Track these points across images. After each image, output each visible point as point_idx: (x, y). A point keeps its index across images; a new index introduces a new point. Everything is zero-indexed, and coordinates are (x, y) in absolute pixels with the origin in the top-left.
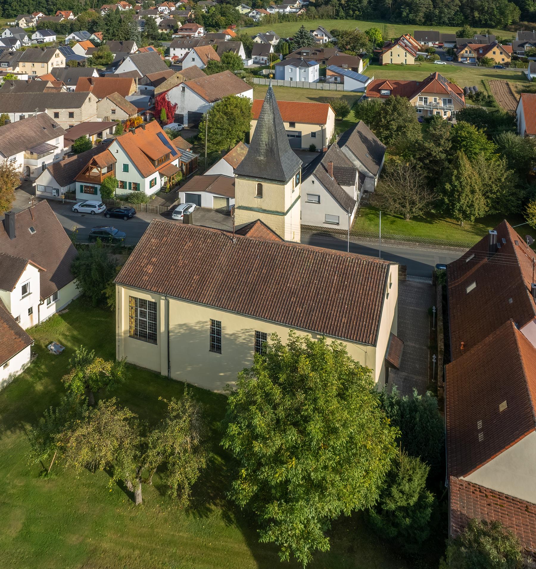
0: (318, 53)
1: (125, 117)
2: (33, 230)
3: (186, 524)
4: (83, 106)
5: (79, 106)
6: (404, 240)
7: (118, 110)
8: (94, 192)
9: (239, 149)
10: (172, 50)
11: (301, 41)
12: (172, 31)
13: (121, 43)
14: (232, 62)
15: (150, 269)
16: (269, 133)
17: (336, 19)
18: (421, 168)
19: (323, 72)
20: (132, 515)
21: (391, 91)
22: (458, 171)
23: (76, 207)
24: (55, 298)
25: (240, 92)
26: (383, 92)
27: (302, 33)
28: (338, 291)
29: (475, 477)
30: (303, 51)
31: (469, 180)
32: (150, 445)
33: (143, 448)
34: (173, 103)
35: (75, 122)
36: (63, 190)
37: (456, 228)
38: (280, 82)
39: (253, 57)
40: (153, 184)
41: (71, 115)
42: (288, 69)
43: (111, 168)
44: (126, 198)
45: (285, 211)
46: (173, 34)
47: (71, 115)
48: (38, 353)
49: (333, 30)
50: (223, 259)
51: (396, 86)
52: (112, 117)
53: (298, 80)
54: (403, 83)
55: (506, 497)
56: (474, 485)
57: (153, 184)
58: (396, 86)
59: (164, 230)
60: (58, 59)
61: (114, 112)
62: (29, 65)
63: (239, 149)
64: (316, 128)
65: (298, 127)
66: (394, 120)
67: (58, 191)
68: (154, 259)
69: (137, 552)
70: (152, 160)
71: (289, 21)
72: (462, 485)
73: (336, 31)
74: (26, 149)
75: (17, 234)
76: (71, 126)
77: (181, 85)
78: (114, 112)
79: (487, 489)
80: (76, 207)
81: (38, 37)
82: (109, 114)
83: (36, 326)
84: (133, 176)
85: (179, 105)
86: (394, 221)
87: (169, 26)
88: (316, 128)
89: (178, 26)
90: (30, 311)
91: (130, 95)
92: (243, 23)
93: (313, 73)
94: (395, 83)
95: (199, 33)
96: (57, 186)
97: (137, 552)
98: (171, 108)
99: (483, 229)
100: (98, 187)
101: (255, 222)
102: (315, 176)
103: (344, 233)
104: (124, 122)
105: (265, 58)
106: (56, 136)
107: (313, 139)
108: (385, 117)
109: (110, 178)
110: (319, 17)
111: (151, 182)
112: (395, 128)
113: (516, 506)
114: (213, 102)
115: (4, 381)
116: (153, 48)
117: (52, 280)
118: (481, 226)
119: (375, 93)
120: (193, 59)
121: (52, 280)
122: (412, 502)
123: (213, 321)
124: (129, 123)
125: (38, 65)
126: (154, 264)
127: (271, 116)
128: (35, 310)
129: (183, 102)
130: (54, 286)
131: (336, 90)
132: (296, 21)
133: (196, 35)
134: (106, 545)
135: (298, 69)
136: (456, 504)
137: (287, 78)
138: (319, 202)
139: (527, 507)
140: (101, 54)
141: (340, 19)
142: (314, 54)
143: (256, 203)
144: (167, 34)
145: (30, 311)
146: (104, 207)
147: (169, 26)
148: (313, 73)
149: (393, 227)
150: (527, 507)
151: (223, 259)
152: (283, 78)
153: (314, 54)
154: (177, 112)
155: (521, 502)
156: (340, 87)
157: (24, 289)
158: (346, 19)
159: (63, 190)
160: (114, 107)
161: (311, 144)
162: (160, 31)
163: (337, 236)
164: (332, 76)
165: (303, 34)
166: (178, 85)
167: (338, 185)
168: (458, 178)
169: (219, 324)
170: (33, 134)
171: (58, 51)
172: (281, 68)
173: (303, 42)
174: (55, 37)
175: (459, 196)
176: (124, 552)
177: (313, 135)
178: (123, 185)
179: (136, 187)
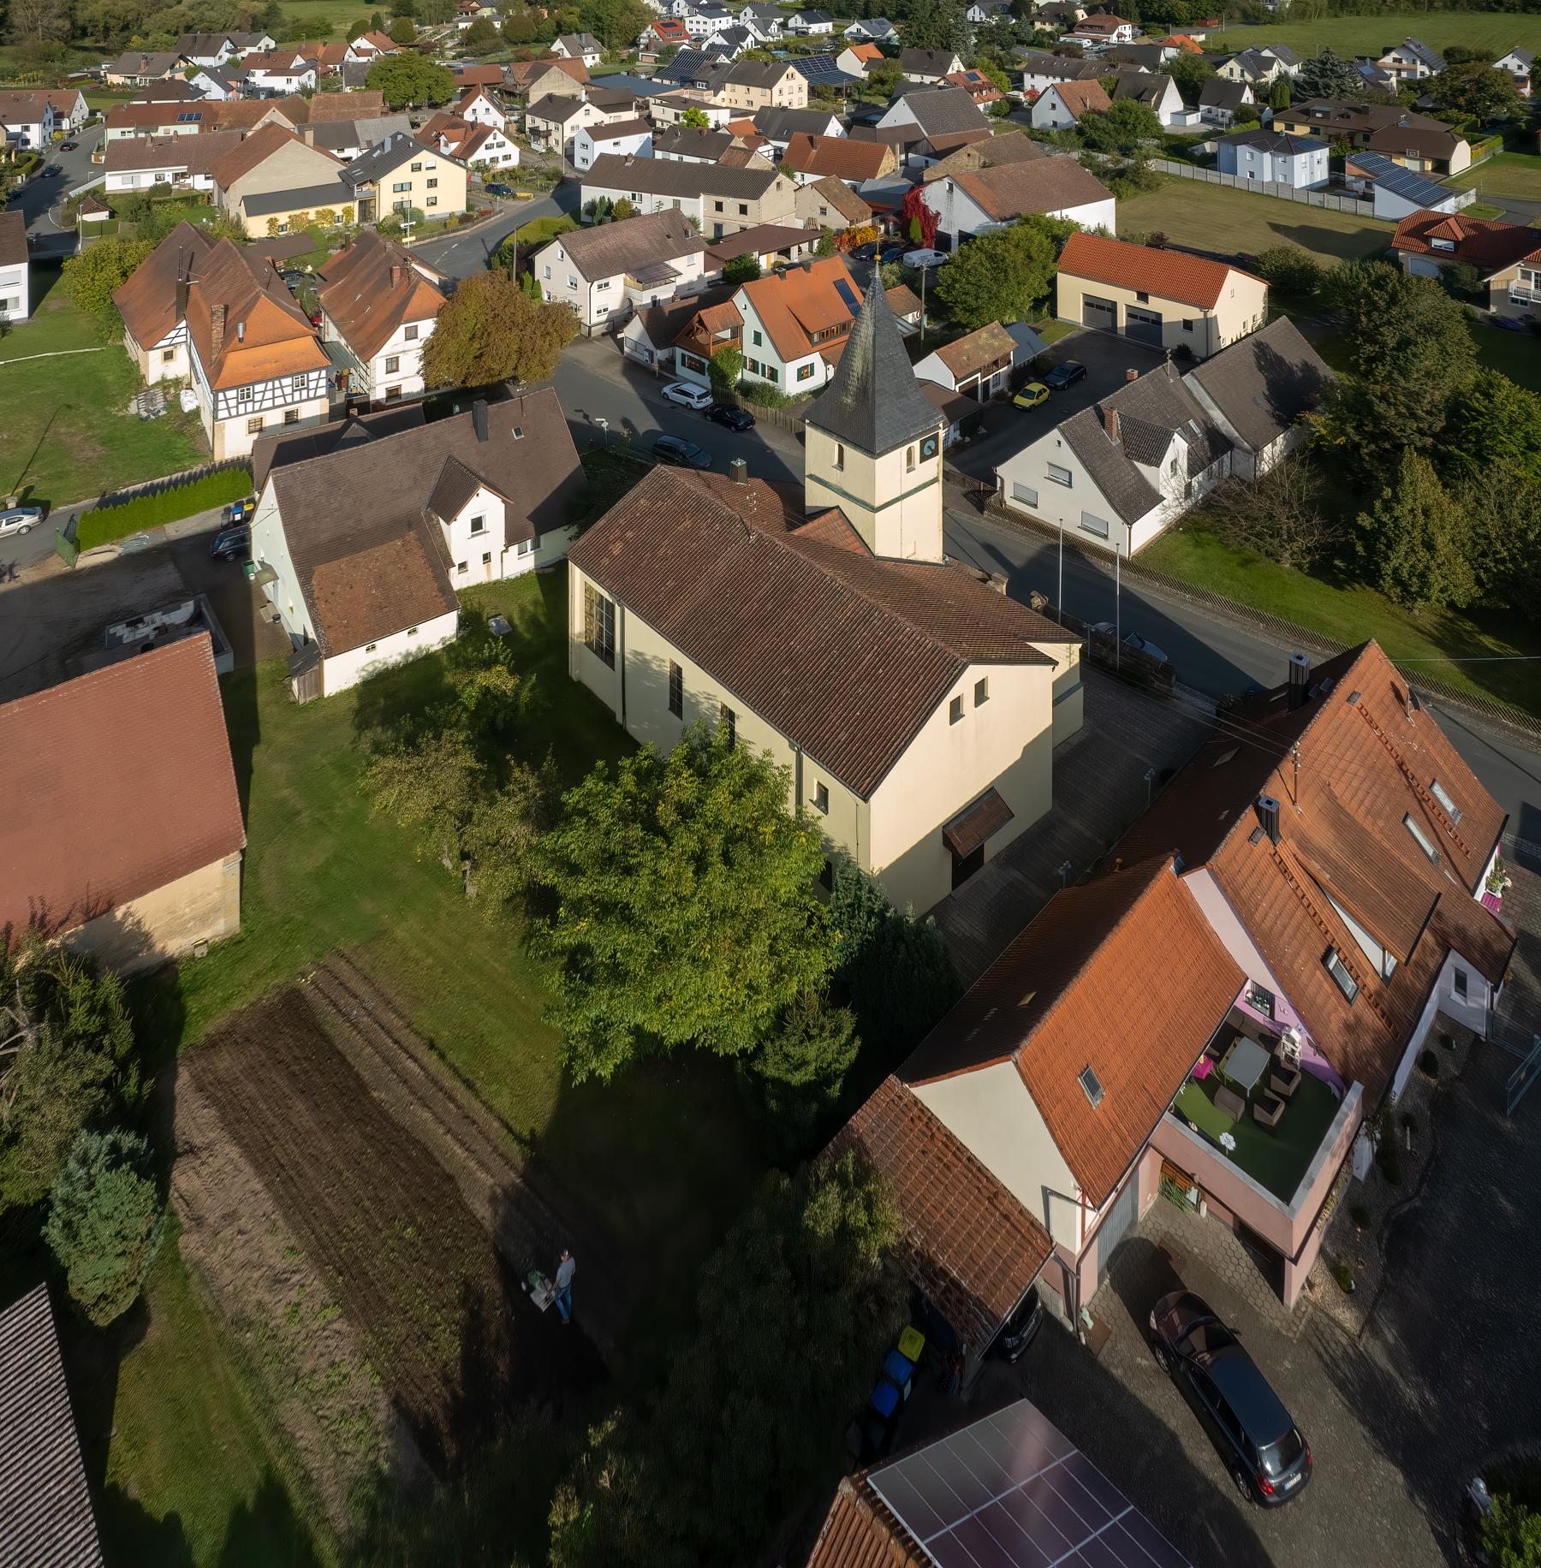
0: (1353, 114)
1: (844, 223)
2: (518, 432)
3: (511, 954)
4: (764, 197)
5: (756, 195)
6: (1232, 607)
7: (830, 209)
8: (700, 369)
9: (984, 335)
10: (1027, 77)
11: (1321, 82)
12: (1065, 28)
13: (930, 54)
14: (1131, 121)
15: (617, 548)
16: (865, 360)
17: (1495, 11)
18: (1370, 454)
19: (1336, 164)
20: (454, 909)
21: (1457, 243)
22: (1395, 494)
23: (666, 390)
24: (536, 546)
25: (1061, 208)
26: (1435, 242)
27: (1324, 64)
28: (859, 681)
29: (931, 1094)
30: (1316, 108)
31: (1421, 519)
32: (475, 818)
33: (466, 818)
34: (933, 209)
35: (750, 222)
36: (660, 355)
37: (1394, 615)
38: (1226, 179)
39: (1203, 107)
40: (804, 373)
41: (743, 210)
42: (1244, 153)
43: (737, 332)
44: (747, 389)
45: (877, 505)
46: (1063, 34)
47: (743, 210)
48: (471, 623)
49: (1452, 49)
50: (721, 566)
51: (1473, 232)
52: (821, 220)
53: (1267, 178)
54: (1494, 228)
55: (969, 1159)
56: (924, 1110)
57: (804, 373)
58: (1473, 232)
59: (664, 487)
60: (791, 83)
61: (823, 211)
62: (741, 89)
63: (984, 335)
64: (1194, 313)
65: (1155, 304)
66: (1390, 323)
67: (651, 354)
68: (629, 534)
69: (430, 961)
70: (809, 335)
71: (1358, 13)
72: (900, 1098)
73: (1460, 51)
74: (627, 271)
75: (491, 433)
76: (743, 229)
77: (946, 180)
78: (823, 211)
79: (941, 1128)
80: (666, 390)
81: (799, 24)
82: (816, 214)
83: (495, 583)
84: (766, 354)
85: (943, 216)
86: (1252, 561)
87: (1058, 16)
88: (1194, 313)
89: (1076, 17)
90: (486, 557)
91: (879, 176)
92: (1238, 14)
93: (1310, 168)
94: (1472, 226)
95: (1120, 35)
96: (651, 347)
97: (430, 961)
98: (930, 220)
99: (1465, 636)
100: (707, 363)
101: (829, 510)
102: (1063, 432)
103: (1110, 557)
104: (840, 232)
105: (1229, 113)
106: (687, 250)
107: (1187, 333)
108: (1368, 314)
109: (728, 350)
110: (1445, 7)
111: (799, 370)
112: (1392, 343)
113: (975, 1181)
114: (1003, 220)
115: (408, 654)
116: (980, 75)
117: (530, 518)
118: (1469, 626)
119: (1414, 241)
120: (1054, 106)
121: (530, 518)
122: (797, 1078)
123: (673, 664)
124: (846, 237)
125: (756, 92)
126: (626, 542)
127: (871, 329)
128: (495, 557)
129: (950, 210)
130: (531, 527)
131: (1356, 214)
132: (1379, 13)
133: (1114, 39)
134: (400, 933)
135: (1267, 156)
136: (862, 1121)
137: (1243, 172)
138: (1070, 486)
139: (996, 1195)
140: (884, 75)
141: (1508, 10)
142: (1342, 116)
143: (834, 477)
144: (1050, 35)
145: (486, 557)
146: (709, 400)
147: (1058, 16)
148: (1310, 168)
149: (1241, 572)
150: (996, 1195)
151: (721, 566)
152: (1234, 172)
153: (1342, 116)
154: (941, 228)
155: (992, 1180)
156: (1363, 207)
157: (477, 524)
158: (1525, 11)
159: (660, 355)
160: (824, 203)
161: (1180, 343)
162: (1038, 25)
163: (1094, 560)
164: (1360, 177)
165: (1329, 66)
166: (940, 179)
167: (1123, 459)
168: (1388, 508)
169: (679, 670)
170: (645, 245)
171: (791, 69)
172: (1231, 148)
173: (1327, 86)
174: (830, 25)
175: (1389, 546)
176: (415, 952)
177: (1188, 325)
178: (754, 367)
179: (774, 374)
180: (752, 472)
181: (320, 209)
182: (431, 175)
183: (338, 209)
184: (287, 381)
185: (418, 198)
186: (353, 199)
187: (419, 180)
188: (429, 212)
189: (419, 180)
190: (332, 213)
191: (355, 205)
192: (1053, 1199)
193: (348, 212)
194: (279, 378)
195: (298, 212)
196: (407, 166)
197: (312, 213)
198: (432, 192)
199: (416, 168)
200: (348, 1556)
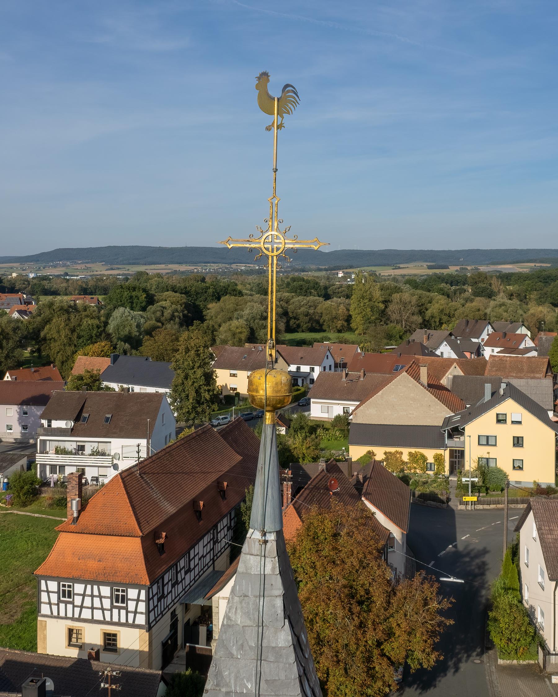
180: (71, 451)
181: (413, 450)
182: (517, 431)
183: (430, 454)
184: (106, 591)
185: (503, 457)
186: (445, 446)
187: (504, 434)
188: (514, 477)
189: (504, 434)
190: (424, 458)
191: (447, 454)
192: (49, 613)
193: (439, 459)
194: (100, 583)
195: (392, 450)
196: (490, 416)
197: (405, 453)
198: (518, 453)
199: (501, 420)
200: (1, 286)
